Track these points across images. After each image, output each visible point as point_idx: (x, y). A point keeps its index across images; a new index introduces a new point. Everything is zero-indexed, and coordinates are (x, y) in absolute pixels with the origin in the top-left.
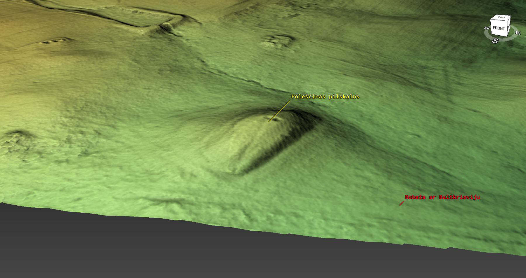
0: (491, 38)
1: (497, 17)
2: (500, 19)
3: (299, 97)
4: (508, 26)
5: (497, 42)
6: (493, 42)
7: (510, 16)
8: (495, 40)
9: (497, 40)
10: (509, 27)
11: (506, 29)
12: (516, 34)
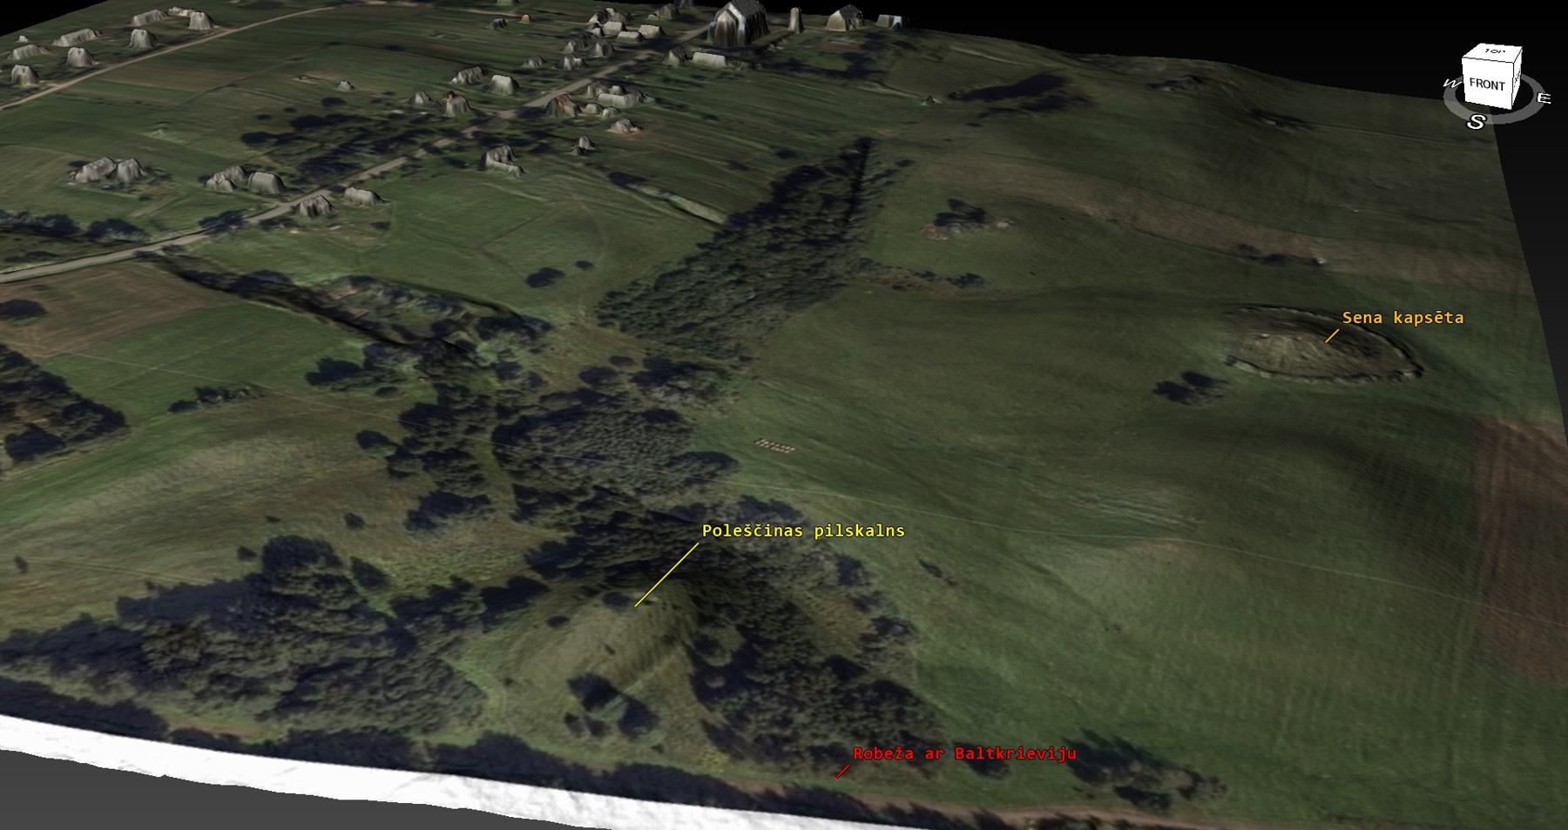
0: (1462, 113)
1: (1481, 49)
2: (1490, 55)
3: (724, 532)
4: (1516, 77)
5: (1481, 125)
6: (1469, 124)
7: (1520, 48)
8: (1476, 118)
9: (1481, 121)
10: (1519, 80)
11: (1508, 87)
12: (1539, 100)
